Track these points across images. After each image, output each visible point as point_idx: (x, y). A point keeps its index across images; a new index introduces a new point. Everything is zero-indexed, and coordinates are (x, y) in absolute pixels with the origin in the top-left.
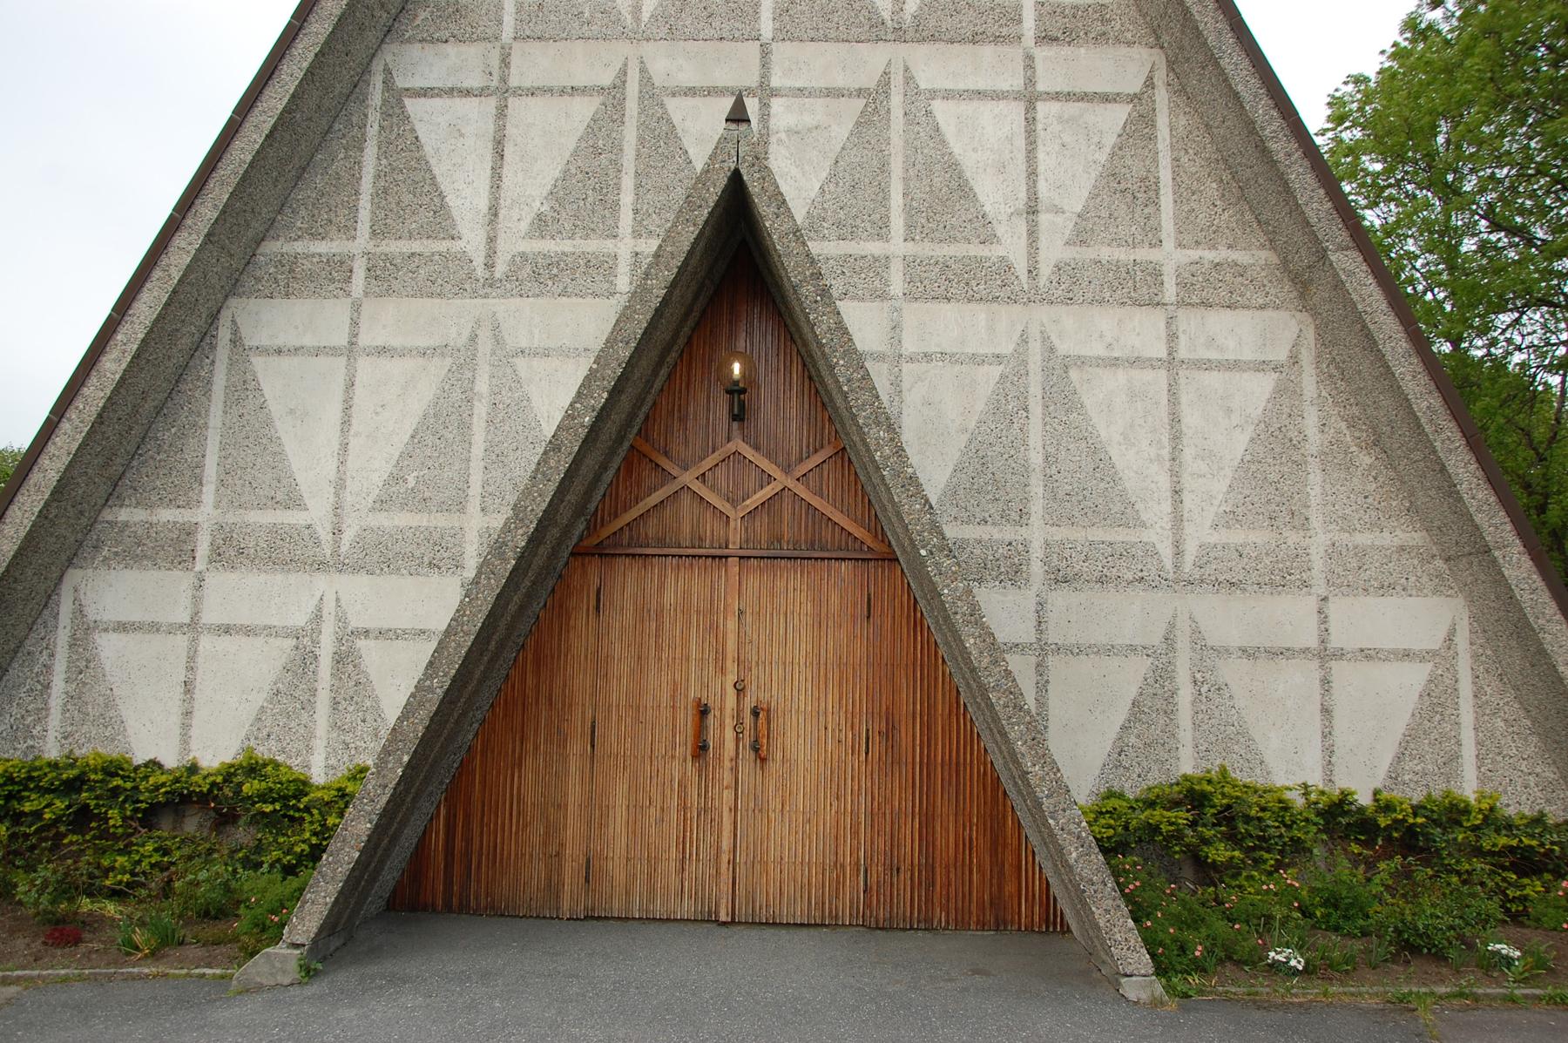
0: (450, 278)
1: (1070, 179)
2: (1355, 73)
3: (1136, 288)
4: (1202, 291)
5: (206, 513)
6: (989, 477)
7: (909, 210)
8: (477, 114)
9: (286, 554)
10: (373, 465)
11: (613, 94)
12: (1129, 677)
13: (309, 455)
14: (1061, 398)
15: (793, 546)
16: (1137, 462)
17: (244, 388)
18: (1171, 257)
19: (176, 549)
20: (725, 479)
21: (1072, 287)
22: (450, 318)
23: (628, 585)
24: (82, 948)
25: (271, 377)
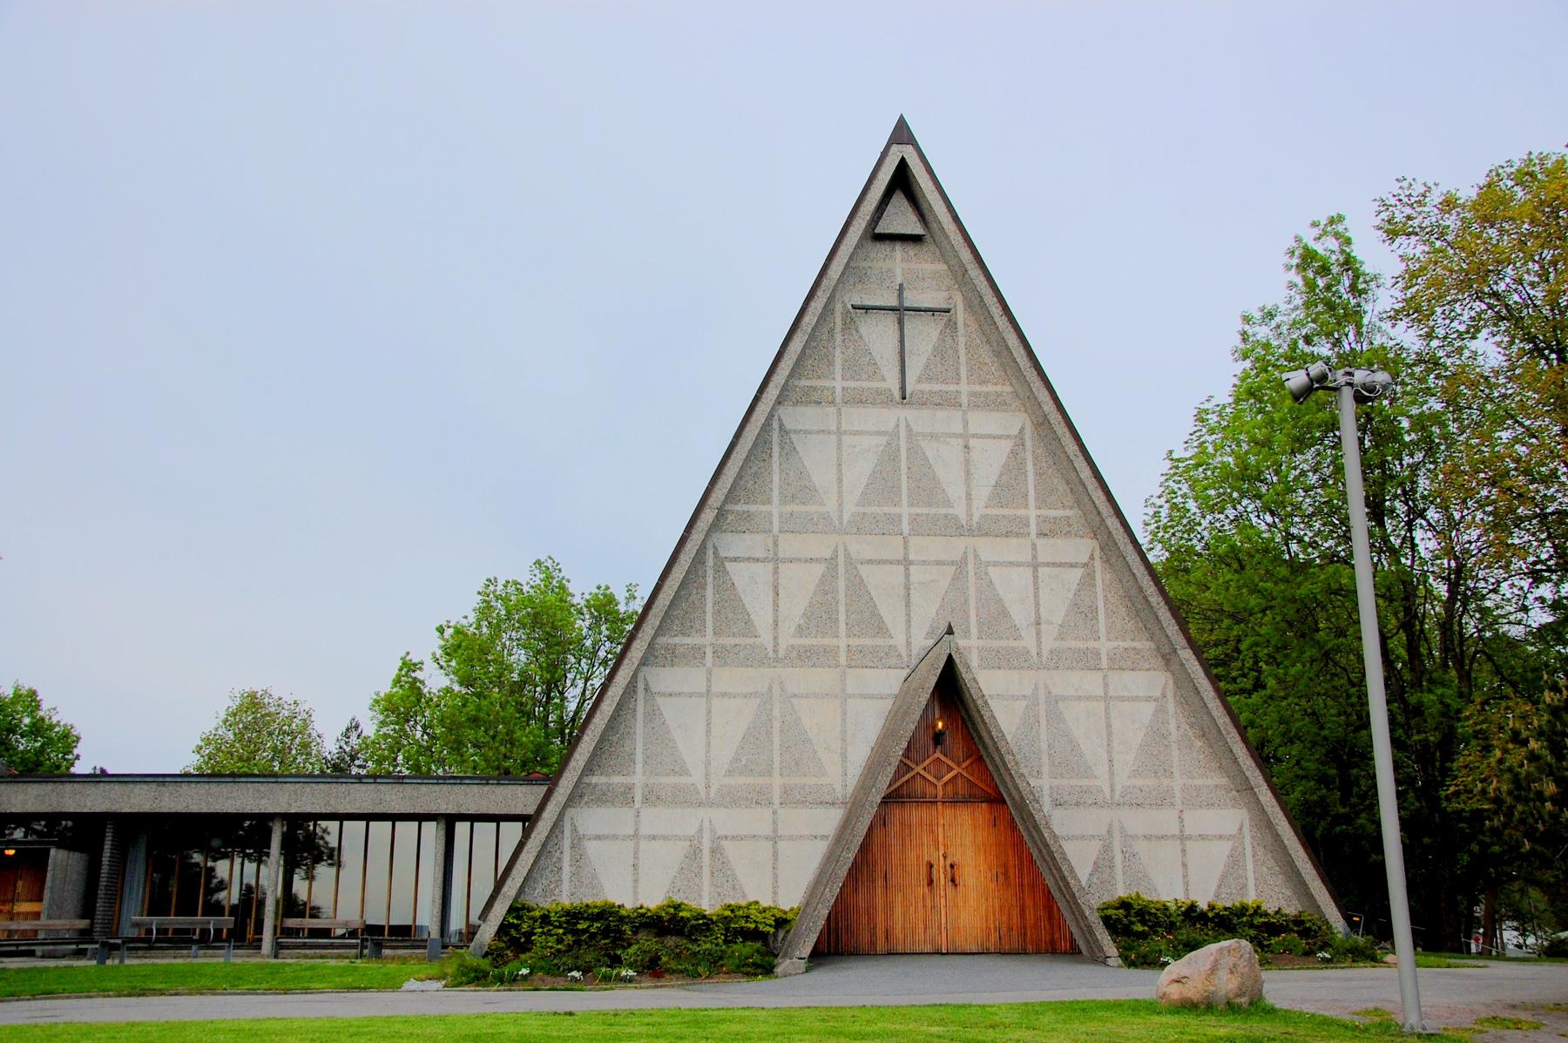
3: (1088, 660)
4: (1120, 662)
5: (638, 778)
9: (682, 798)
13: (690, 747)
17: (653, 714)
18: (964, 388)
19: (625, 797)
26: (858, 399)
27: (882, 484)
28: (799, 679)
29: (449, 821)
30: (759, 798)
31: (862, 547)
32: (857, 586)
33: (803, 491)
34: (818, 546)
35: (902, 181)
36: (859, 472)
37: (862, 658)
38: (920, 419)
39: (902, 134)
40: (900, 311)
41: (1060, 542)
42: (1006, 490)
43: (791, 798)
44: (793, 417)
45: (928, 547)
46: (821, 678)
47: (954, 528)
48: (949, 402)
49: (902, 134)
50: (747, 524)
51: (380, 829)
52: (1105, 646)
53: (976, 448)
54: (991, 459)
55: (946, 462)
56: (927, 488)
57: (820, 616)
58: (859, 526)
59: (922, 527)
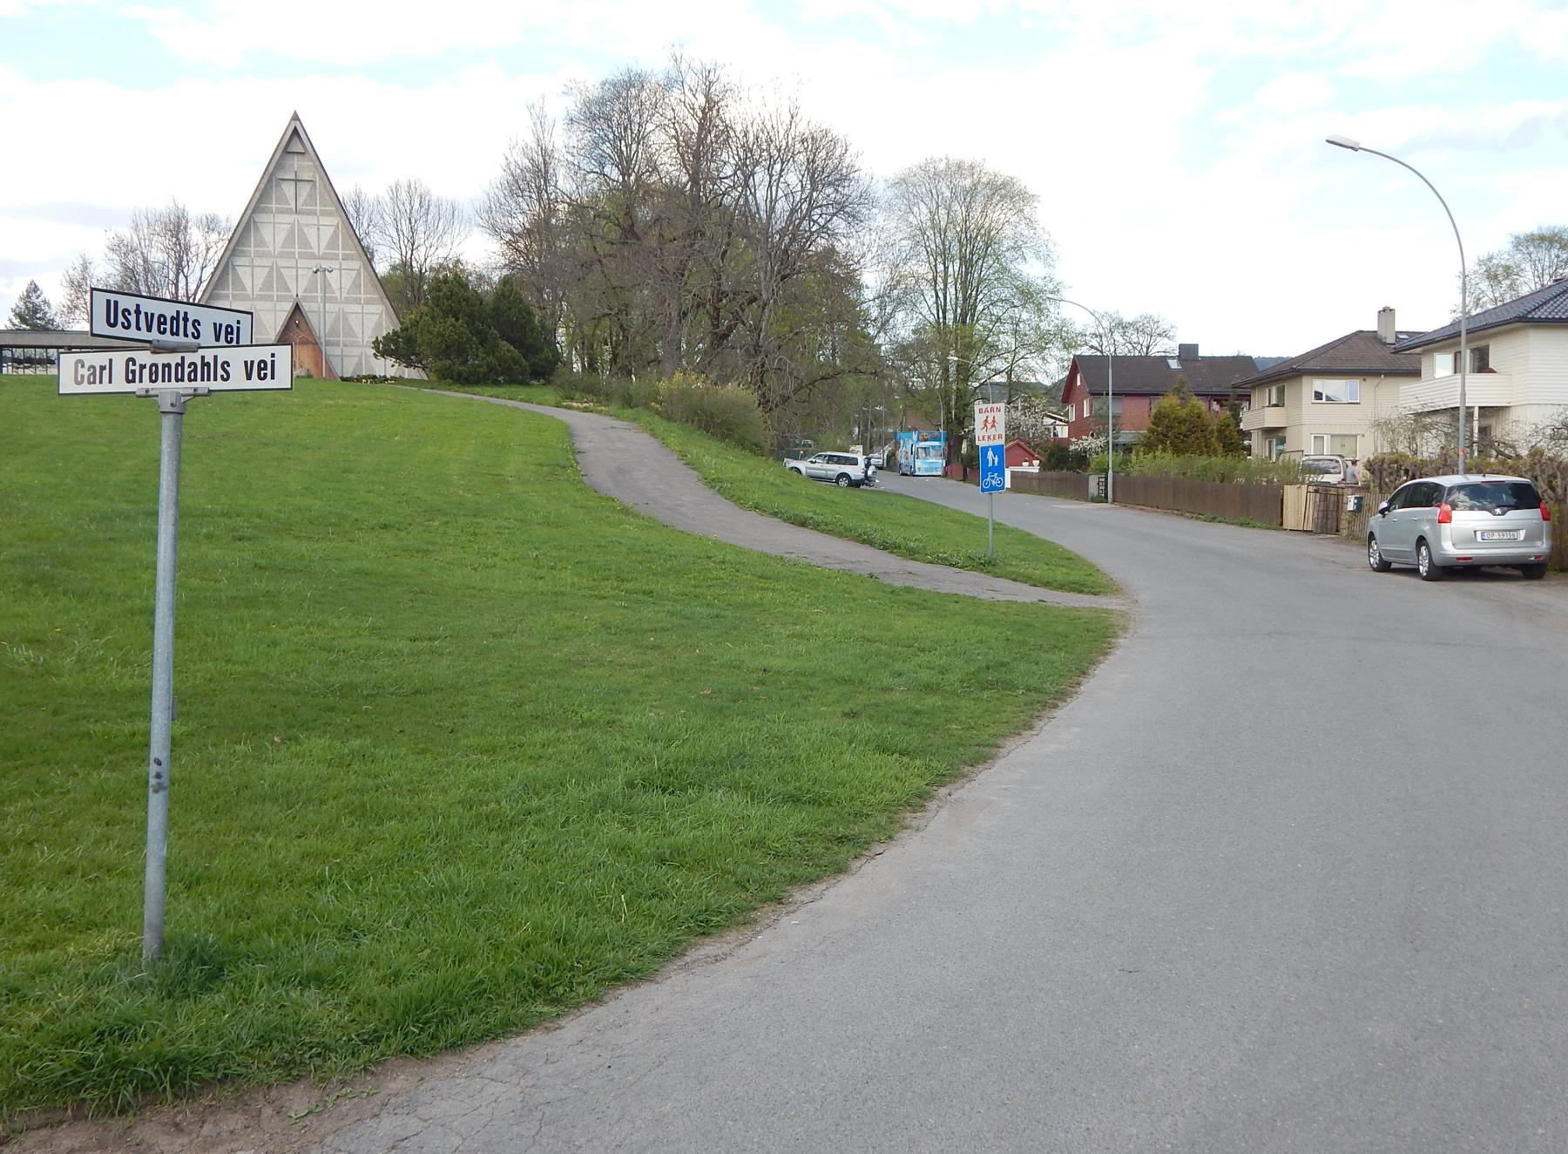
0: (268, 255)
1: (347, 284)
2: (1111, 311)
3: (357, 301)
4: (368, 302)
7: (182, 514)
8: (248, 270)
11: (271, 268)
12: (355, 360)
14: (345, 319)
20: (297, 315)
21: (347, 301)
25: (240, 270)
26: (281, 212)
27: (289, 240)
31: (281, 262)
32: (280, 275)
33: (262, 243)
34: (267, 262)
35: (295, 131)
36: (281, 237)
37: (280, 299)
38: (303, 219)
39: (296, 117)
41: (390, 361)
42: (332, 244)
45: (303, 263)
46: (268, 305)
47: (313, 256)
48: (313, 213)
49: (296, 117)
50: (243, 253)
52: (363, 296)
53: (321, 231)
54: (327, 233)
55: (311, 235)
56: (305, 243)
57: (268, 285)
58: (281, 255)
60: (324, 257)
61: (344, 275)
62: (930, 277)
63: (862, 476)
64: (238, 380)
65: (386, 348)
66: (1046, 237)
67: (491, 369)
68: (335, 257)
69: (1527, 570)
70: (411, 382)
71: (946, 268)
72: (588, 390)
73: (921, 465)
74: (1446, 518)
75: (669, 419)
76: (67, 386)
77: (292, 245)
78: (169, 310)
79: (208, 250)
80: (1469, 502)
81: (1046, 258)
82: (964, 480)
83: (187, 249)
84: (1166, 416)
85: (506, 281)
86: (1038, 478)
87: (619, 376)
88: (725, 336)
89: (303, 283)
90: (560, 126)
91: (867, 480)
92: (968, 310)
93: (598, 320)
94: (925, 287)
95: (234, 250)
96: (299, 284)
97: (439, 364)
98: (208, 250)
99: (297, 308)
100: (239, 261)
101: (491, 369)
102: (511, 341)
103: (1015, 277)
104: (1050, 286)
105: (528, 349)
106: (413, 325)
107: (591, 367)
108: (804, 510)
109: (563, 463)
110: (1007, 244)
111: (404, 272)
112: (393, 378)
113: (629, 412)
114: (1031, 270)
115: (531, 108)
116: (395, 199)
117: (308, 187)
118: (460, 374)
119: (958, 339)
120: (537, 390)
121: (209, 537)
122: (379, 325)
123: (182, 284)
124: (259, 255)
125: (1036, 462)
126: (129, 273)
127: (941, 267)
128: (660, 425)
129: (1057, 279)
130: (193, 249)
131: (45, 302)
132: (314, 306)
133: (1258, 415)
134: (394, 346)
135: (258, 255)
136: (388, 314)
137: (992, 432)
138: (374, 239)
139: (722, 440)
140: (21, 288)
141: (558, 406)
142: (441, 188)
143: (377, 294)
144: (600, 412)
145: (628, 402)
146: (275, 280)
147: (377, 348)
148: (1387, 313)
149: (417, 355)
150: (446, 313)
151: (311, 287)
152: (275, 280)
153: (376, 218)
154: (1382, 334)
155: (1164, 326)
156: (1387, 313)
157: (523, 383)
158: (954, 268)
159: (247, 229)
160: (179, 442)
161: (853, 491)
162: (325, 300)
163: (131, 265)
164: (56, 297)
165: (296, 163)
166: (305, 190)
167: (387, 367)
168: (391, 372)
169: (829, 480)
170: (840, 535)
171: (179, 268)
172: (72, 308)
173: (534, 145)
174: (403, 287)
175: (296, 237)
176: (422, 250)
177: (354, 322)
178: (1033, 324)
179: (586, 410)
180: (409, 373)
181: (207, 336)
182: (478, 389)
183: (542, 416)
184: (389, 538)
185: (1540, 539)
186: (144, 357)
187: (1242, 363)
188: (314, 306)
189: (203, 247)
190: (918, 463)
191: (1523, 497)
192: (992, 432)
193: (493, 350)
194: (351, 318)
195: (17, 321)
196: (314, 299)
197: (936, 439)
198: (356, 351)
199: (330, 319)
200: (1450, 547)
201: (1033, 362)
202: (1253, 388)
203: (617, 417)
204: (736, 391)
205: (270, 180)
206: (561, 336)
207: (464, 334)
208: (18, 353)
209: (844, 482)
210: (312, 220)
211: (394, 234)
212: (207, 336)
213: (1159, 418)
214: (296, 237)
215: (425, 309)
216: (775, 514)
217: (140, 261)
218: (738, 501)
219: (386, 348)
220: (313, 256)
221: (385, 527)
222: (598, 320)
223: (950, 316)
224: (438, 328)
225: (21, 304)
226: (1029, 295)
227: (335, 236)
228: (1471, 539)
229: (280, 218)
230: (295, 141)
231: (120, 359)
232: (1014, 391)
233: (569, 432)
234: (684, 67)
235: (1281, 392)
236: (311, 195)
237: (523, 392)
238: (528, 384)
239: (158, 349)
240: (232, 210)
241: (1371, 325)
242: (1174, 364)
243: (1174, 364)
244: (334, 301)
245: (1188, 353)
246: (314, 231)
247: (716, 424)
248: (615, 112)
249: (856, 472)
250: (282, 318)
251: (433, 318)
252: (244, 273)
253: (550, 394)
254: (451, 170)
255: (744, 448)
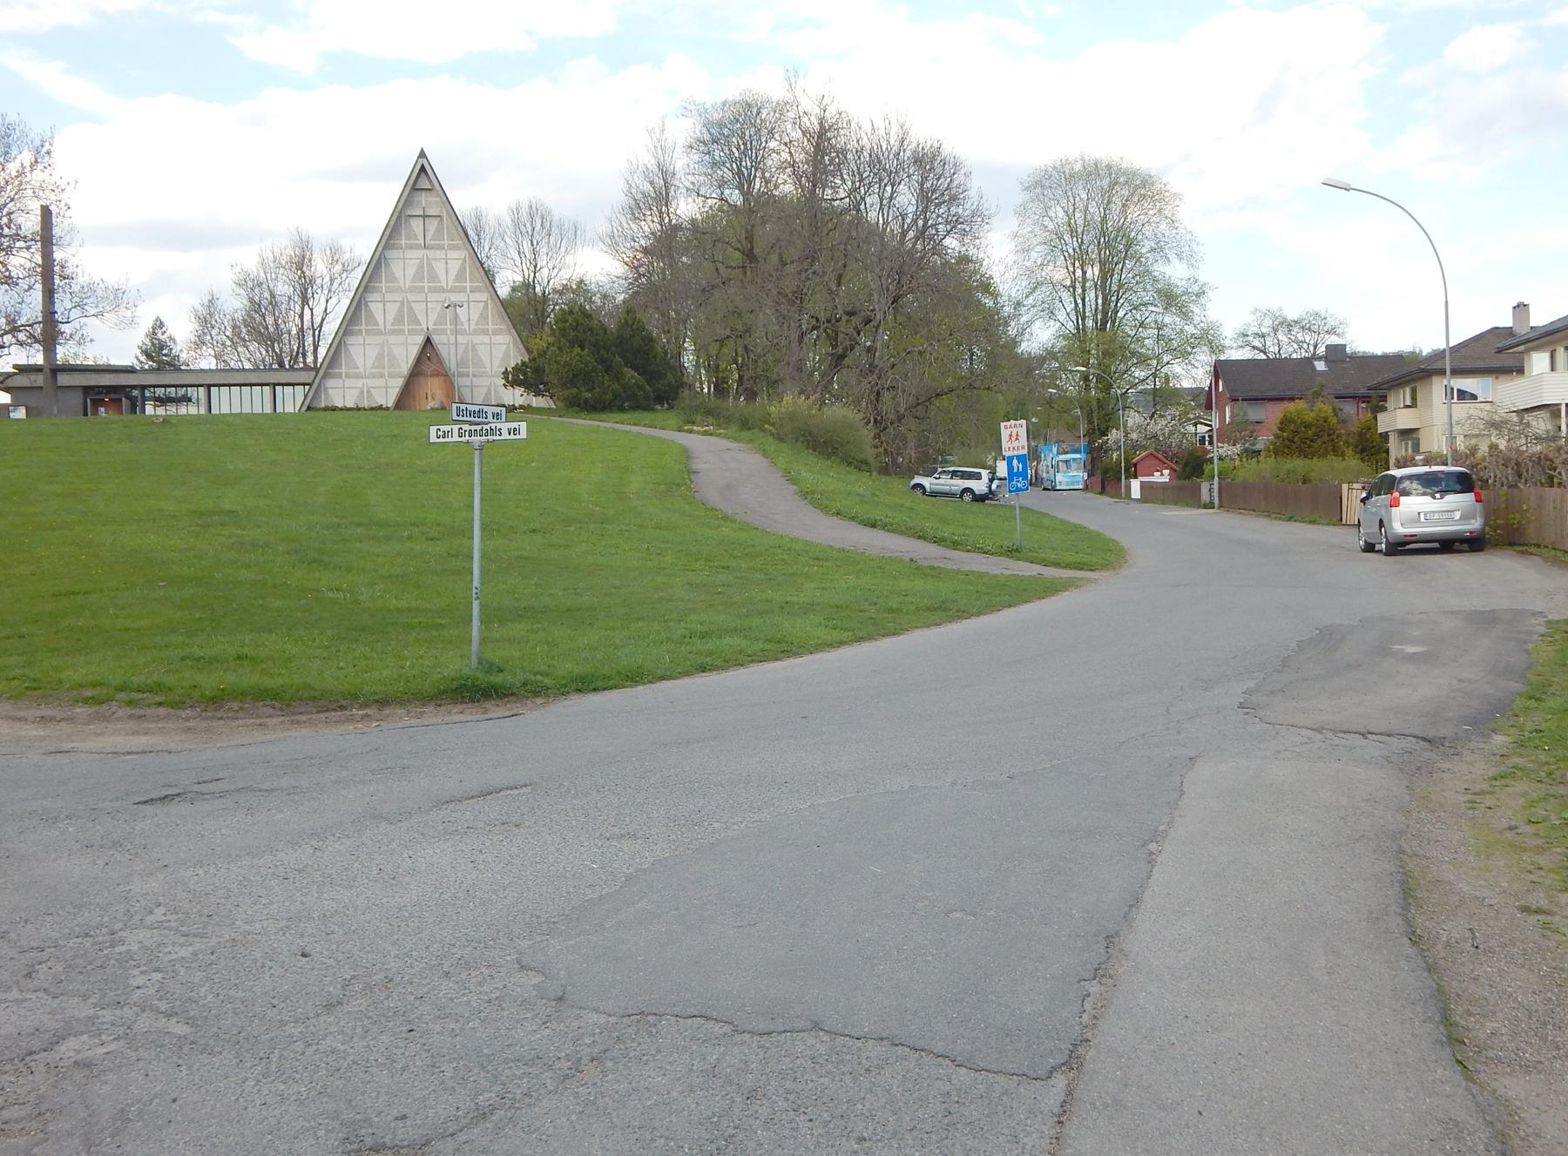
1: (475, 316)
2: (1274, 308)
3: (485, 332)
4: (495, 333)
5: (343, 370)
6: (462, 363)
9: (358, 376)
10: (370, 363)
12: (484, 390)
13: (359, 361)
14: (474, 349)
15: (436, 374)
16: (485, 359)
17: (347, 350)
18: (491, 327)
19: (339, 376)
20: (429, 349)
22: (380, 339)
23: (422, 379)
24: (1333, 340)
26: (410, 247)
27: (418, 276)
28: (392, 339)
29: (209, 386)
30: (382, 376)
31: (411, 297)
32: (411, 309)
33: (393, 278)
34: (398, 297)
35: (423, 168)
36: (411, 272)
37: (411, 332)
38: (431, 254)
39: (422, 155)
40: (424, 216)
41: (519, 391)
42: (460, 276)
43: (390, 376)
44: (391, 254)
45: (433, 297)
46: (400, 339)
47: (443, 290)
48: (441, 247)
49: (422, 155)
50: (375, 290)
51: (246, 389)
52: (491, 327)
53: (450, 263)
54: (455, 266)
55: (439, 268)
56: (434, 277)
57: (399, 319)
58: (411, 290)
59: (432, 290)
60: (452, 290)
61: (475, 308)
62: (1068, 283)
63: (986, 490)
64: (505, 436)
65: (515, 378)
66: (1189, 236)
67: (616, 395)
68: (463, 290)
69: (1447, 545)
70: (539, 410)
71: (1084, 273)
72: (711, 415)
73: (1062, 479)
74: (1395, 504)
75: (781, 440)
76: (433, 439)
77: (422, 280)
78: (477, 408)
79: (332, 280)
80: (1421, 489)
81: (1190, 259)
82: (1103, 492)
83: (312, 282)
84: (1292, 421)
85: (629, 309)
86: (1163, 487)
87: (739, 397)
88: (843, 357)
89: (433, 317)
90: (679, 150)
91: (989, 496)
92: (1107, 315)
93: (722, 342)
94: (1066, 295)
95: (366, 287)
96: (429, 317)
97: (567, 392)
98: (332, 280)
99: (428, 341)
100: (371, 297)
101: (616, 395)
102: (635, 368)
103: (1155, 280)
104: (1195, 288)
105: (651, 376)
106: (540, 355)
107: (721, 389)
108: (877, 514)
109: (679, 480)
110: (1148, 245)
111: (527, 294)
112: (521, 407)
113: (746, 434)
114: (1174, 272)
115: (650, 132)
116: (517, 223)
117: (435, 222)
118: (586, 401)
119: (1101, 344)
120: (661, 415)
121: (410, 537)
122: (506, 355)
123: (307, 317)
124: (390, 290)
125: (1166, 472)
126: (255, 306)
127: (1079, 273)
128: (772, 445)
129: (1202, 279)
130: (318, 281)
131: (171, 338)
132: (444, 338)
133: (1396, 417)
134: (525, 376)
135: (389, 290)
136: (515, 344)
137: (1015, 444)
138: (495, 262)
139: (829, 458)
140: (146, 324)
141: (680, 430)
142: (561, 206)
143: (504, 325)
144: (719, 435)
145: (745, 425)
146: (406, 314)
147: (506, 378)
148: (1521, 309)
149: (545, 384)
150: (572, 344)
151: (441, 320)
152: (406, 314)
153: (497, 241)
154: (1518, 330)
155: (1331, 322)
156: (1521, 309)
157: (648, 408)
158: (1093, 272)
159: (379, 263)
160: (481, 463)
161: (978, 506)
162: (456, 332)
163: (257, 299)
164: (181, 332)
165: (424, 198)
166: (432, 225)
167: (517, 396)
168: (519, 401)
169: (953, 495)
170: (902, 533)
171: (305, 301)
172: (200, 343)
173: (655, 169)
174: (525, 310)
175: (425, 272)
176: (545, 272)
177: (483, 353)
178: (1178, 329)
179: (706, 433)
180: (536, 402)
181: (490, 418)
182: (604, 416)
183: (663, 440)
184: (538, 538)
185: (1474, 517)
186: (466, 427)
187: (1397, 359)
188: (444, 338)
189: (327, 279)
190: (1059, 477)
191: (1464, 483)
192: (1015, 444)
193: (618, 377)
194: (479, 348)
195: (143, 358)
196: (443, 332)
197: (1077, 451)
198: (485, 382)
199: (461, 349)
200: (1399, 528)
201: (1177, 368)
202: (1389, 389)
203: (735, 439)
204: (839, 413)
205: (399, 217)
206: (688, 359)
207: (592, 360)
208: (160, 392)
209: (967, 497)
210: (440, 254)
211: (517, 257)
212: (490, 418)
213: (1285, 423)
214: (425, 272)
215: (551, 339)
216: (853, 519)
217: (267, 295)
218: (825, 509)
219: (515, 378)
220: (443, 290)
221: (534, 531)
222: (722, 342)
223: (1090, 323)
224: (564, 358)
225: (147, 341)
226: (1170, 298)
227: (462, 269)
228: (1416, 520)
229: (410, 253)
230: (422, 178)
231: (455, 428)
232: (1163, 397)
233: (687, 454)
234: (798, 92)
235: (1414, 392)
236: (439, 230)
237: (647, 417)
238: (652, 409)
239: (472, 423)
240: (363, 249)
241: (1506, 321)
242: (1320, 366)
243: (1320, 366)
244: (464, 332)
245: (1336, 354)
246: (442, 265)
247: (825, 444)
248: (736, 135)
249: (979, 486)
250: (414, 351)
251: (559, 348)
252: (376, 308)
253: (672, 418)
254: (577, 176)
255: (850, 464)
